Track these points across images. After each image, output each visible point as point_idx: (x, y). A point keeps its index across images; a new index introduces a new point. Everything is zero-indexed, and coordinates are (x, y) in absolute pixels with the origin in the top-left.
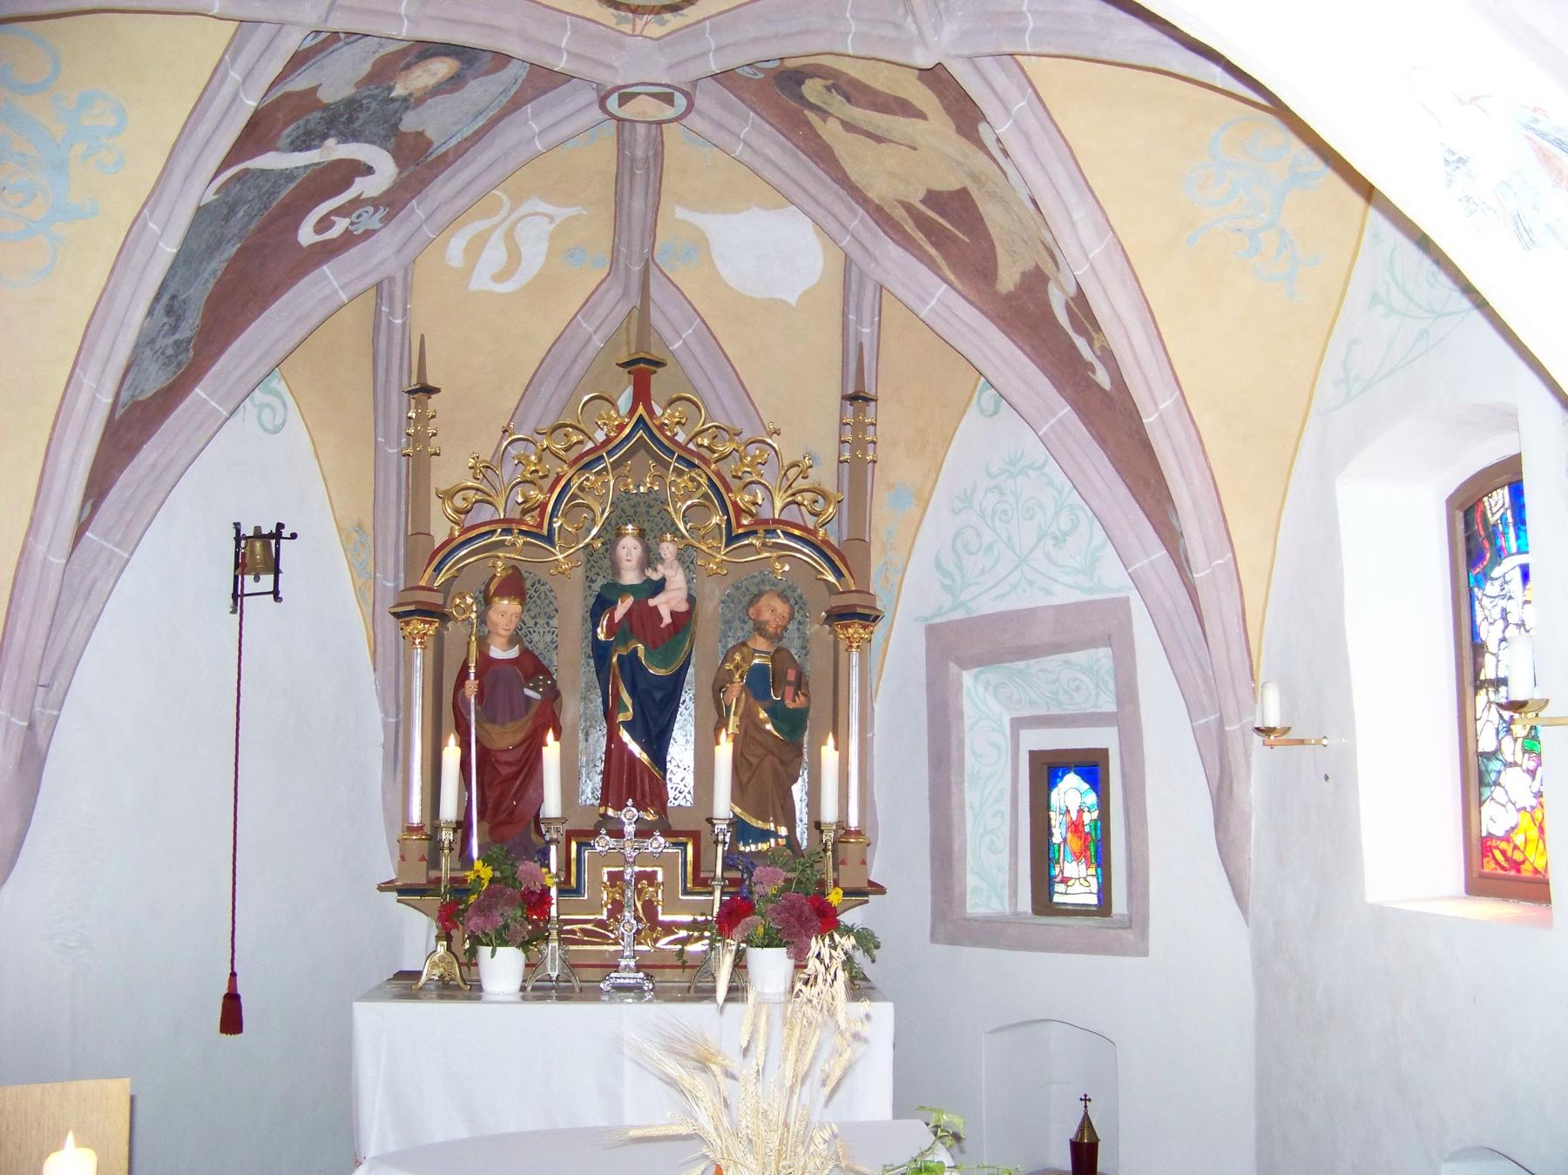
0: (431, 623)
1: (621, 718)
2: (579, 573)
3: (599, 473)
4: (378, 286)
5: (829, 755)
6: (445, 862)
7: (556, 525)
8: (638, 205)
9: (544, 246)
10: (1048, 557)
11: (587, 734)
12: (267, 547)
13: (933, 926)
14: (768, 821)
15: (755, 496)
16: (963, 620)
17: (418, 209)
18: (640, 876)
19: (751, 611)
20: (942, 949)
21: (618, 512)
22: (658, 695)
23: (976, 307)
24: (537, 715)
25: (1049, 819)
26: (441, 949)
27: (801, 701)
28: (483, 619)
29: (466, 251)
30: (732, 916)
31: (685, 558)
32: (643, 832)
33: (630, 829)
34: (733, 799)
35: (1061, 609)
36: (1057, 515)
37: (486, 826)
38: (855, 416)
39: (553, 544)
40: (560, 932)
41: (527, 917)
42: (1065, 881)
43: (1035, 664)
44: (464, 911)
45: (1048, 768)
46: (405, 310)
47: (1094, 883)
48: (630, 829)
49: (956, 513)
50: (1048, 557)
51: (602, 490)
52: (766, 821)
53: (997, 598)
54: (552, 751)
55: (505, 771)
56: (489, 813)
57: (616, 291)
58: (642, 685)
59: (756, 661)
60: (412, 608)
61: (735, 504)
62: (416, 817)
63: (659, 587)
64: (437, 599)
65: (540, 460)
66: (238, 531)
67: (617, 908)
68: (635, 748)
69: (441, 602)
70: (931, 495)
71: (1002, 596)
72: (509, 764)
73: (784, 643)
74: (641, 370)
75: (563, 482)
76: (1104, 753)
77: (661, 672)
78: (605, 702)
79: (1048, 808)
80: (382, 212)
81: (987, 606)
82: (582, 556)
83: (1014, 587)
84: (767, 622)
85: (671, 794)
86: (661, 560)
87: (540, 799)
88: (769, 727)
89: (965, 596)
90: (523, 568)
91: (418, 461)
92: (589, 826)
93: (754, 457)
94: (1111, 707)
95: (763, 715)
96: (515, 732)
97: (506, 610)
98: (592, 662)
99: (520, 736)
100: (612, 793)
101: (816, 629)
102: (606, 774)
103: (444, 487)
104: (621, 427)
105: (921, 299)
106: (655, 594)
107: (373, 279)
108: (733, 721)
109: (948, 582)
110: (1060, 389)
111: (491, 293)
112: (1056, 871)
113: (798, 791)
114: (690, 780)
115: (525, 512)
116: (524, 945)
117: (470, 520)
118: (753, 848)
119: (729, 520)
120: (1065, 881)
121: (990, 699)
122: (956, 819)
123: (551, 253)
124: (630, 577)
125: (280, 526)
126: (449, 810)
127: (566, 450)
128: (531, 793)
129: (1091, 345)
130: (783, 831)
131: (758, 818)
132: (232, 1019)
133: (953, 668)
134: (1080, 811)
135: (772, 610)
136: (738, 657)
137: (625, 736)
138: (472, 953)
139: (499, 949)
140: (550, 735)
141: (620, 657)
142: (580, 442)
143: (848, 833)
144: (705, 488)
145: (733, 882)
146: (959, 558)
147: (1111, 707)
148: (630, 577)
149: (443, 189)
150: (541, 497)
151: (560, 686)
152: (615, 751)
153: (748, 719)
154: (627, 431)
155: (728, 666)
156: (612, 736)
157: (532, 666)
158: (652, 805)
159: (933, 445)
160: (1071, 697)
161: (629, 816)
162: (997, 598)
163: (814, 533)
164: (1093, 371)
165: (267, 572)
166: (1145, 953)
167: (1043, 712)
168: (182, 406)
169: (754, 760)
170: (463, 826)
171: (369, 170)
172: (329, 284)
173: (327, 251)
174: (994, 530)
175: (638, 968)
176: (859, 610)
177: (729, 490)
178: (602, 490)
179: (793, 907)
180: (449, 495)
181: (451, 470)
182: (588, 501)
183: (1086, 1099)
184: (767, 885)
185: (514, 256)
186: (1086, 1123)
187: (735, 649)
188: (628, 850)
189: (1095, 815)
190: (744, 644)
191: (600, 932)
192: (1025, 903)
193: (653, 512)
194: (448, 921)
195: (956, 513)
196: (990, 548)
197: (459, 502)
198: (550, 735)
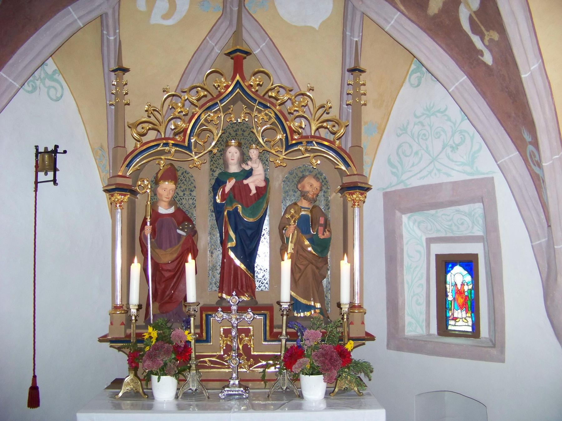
0: (125, 195)
1: (229, 245)
2: (207, 167)
3: (215, 112)
5: (345, 265)
7: (192, 141)
10: (449, 157)
11: (212, 253)
14: (310, 300)
15: (301, 123)
16: (403, 190)
19: (299, 186)
20: (393, 353)
21: (227, 134)
22: (249, 232)
23: (416, 24)
24: (184, 244)
25: (446, 288)
30: (292, 357)
31: (263, 157)
33: (234, 308)
34: (292, 289)
36: (453, 135)
37: (157, 305)
38: (355, 79)
39: (191, 152)
41: (180, 360)
43: (440, 212)
44: (143, 355)
45: (445, 263)
48: (234, 308)
49: (398, 136)
50: (449, 157)
51: (218, 120)
53: (421, 178)
54: (190, 265)
55: (167, 274)
56: (159, 298)
57: (225, 24)
58: (241, 227)
59: (303, 213)
60: (114, 187)
61: (290, 128)
62: (119, 302)
63: (249, 173)
64: (129, 182)
65: (183, 106)
66: (37, 150)
68: (238, 262)
69: (130, 183)
70: (384, 129)
71: (423, 178)
72: (170, 271)
73: (317, 203)
74: (238, 56)
75: (196, 117)
76: (476, 256)
77: (251, 220)
78: (221, 236)
81: (416, 182)
82: (207, 158)
83: (430, 173)
84: (308, 192)
85: (257, 284)
86: (250, 159)
88: (310, 249)
89: (404, 177)
90: (176, 165)
91: (118, 105)
93: (300, 102)
94: (481, 233)
95: (307, 243)
96: (171, 254)
97: (167, 188)
98: (214, 214)
99: (175, 256)
101: (335, 197)
104: (227, 87)
105: (385, 20)
106: (247, 177)
108: (291, 246)
109: (394, 170)
110: (461, 67)
114: (267, 276)
115: (176, 134)
116: (175, 375)
117: (145, 139)
118: (302, 315)
119: (287, 136)
120: (455, 319)
122: (399, 289)
124: (234, 168)
125: (56, 147)
127: (198, 100)
129: (482, 39)
130: (318, 305)
131: (304, 298)
132: (34, 399)
133: (398, 213)
134: (463, 285)
136: (292, 211)
137: (232, 255)
139: (163, 378)
140: (190, 257)
141: (228, 212)
142: (205, 96)
144: (273, 120)
146: (400, 158)
148: (234, 168)
150: (184, 125)
151: (197, 228)
152: (226, 262)
153: (299, 245)
154: (230, 89)
155: (288, 216)
156: (225, 254)
157: (182, 217)
158: (247, 292)
159: (387, 103)
160: (458, 228)
161: (233, 300)
162: (421, 178)
163: (333, 142)
164: (482, 55)
165: (50, 170)
166: (503, 361)
167: (442, 235)
169: (302, 267)
174: (419, 144)
176: (359, 185)
177: (286, 120)
178: (218, 120)
179: (327, 354)
181: (135, 112)
182: (210, 127)
184: (311, 339)
187: (290, 207)
189: (470, 287)
190: (295, 204)
191: (220, 362)
192: (434, 329)
193: (246, 134)
195: (398, 136)
196: (417, 153)
197: (139, 129)
198: (190, 257)
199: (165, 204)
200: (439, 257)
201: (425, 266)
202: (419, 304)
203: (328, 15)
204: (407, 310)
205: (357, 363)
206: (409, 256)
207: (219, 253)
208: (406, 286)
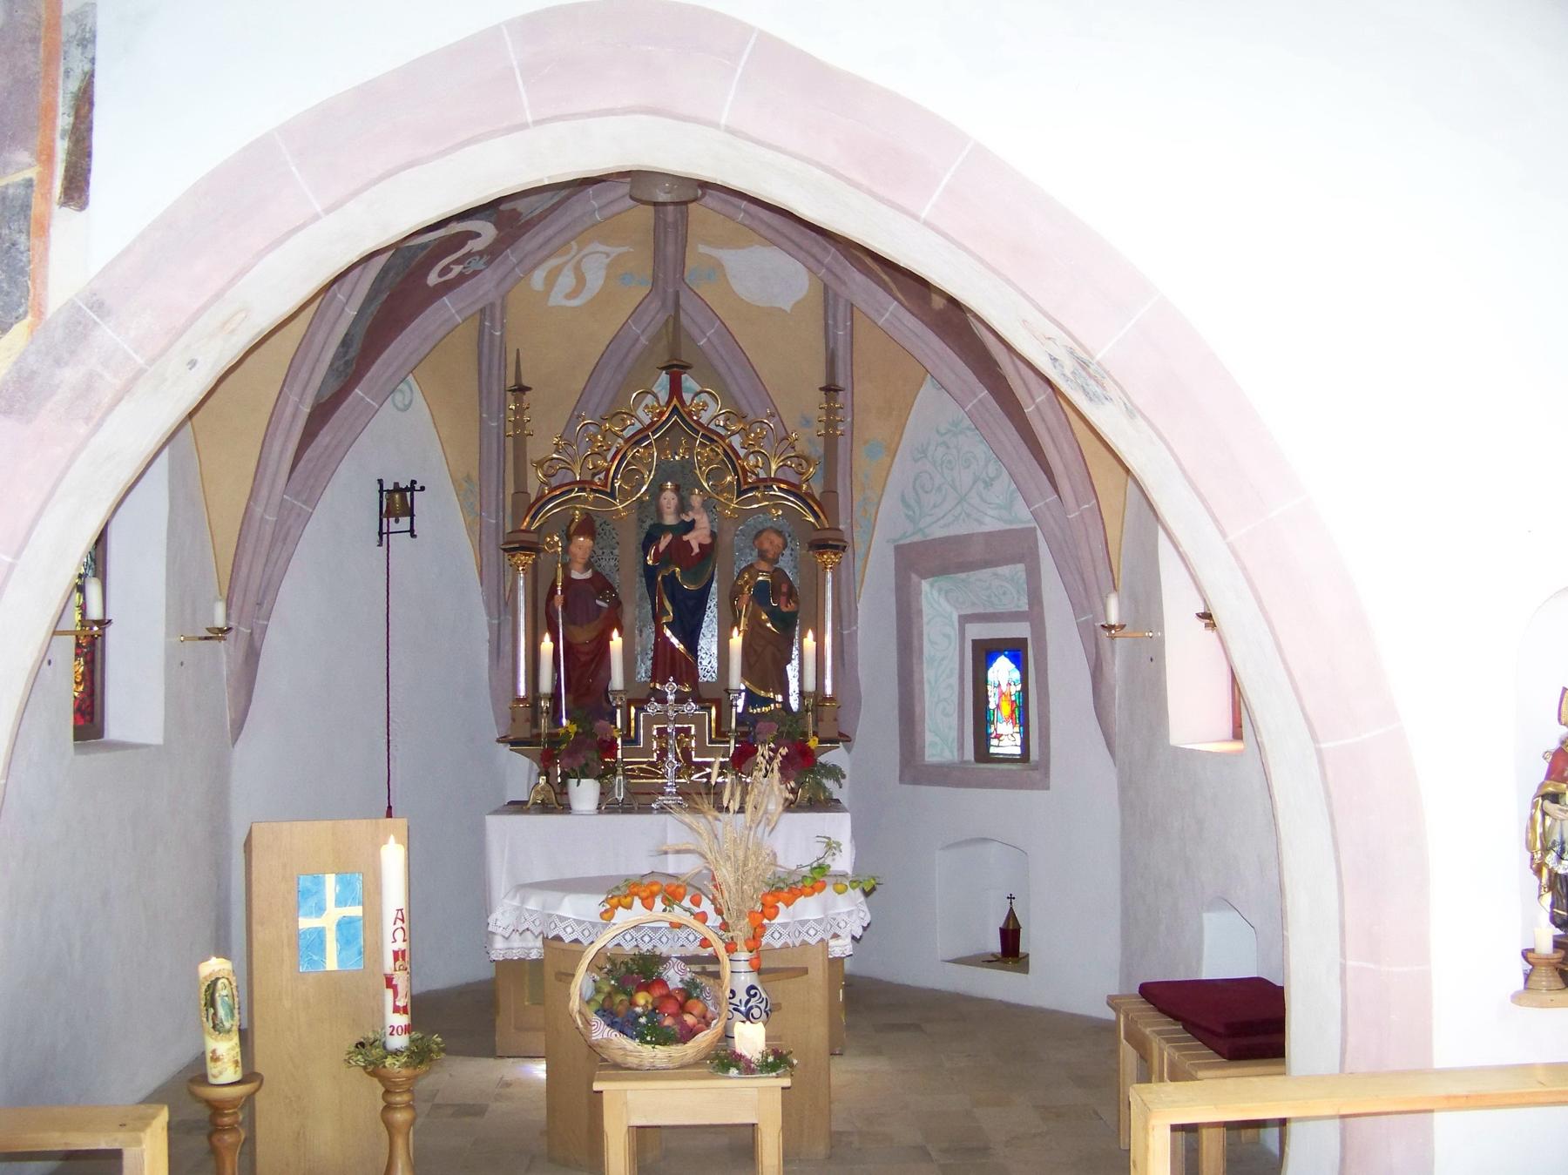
4: (483, 311)
5: (809, 642)
6: (544, 722)
8: (670, 249)
9: (603, 273)
12: (403, 498)
13: (902, 772)
17: (511, 256)
18: (678, 731)
20: (909, 788)
22: (690, 603)
26: (543, 780)
27: (791, 607)
28: (566, 550)
29: (546, 278)
31: (708, 506)
32: (681, 699)
33: (671, 697)
35: (990, 534)
40: (624, 771)
42: (998, 737)
46: (503, 325)
47: (1018, 738)
48: (671, 697)
52: (767, 691)
54: (616, 642)
55: (583, 659)
57: (655, 305)
61: (743, 468)
62: (522, 693)
63: (690, 526)
64: (533, 538)
67: (663, 753)
68: (674, 641)
73: (781, 564)
77: (692, 588)
79: (986, 682)
80: (485, 258)
81: (938, 532)
85: (701, 673)
86: (692, 508)
87: (609, 678)
92: (644, 696)
94: (1026, 608)
95: (764, 617)
99: (594, 634)
100: (658, 674)
102: (655, 659)
103: (539, 456)
104: (661, 414)
107: (479, 306)
111: (562, 307)
112: (992, 730)
113: (792, 670)
120: (998, 737)
121: (942, 601)
122: (917, 691)
123: (607, 277)
124: (670, 520)
125: (413, 482)
126: (546, 685)
128: (602, 674)
130: (779, 698)
133: (914, 577)
135: (771, 542)
137: (668, 633)
138: (564, 784)
140: (615, 633)
143: (825, 699)
145: (744, 734)
147: (1026, 608)
148: (670, 520)
149: (529, 242)
152: (661, 644)
155: (740, 582)
156: (659, 633)
157: (601, 584)
159: (898, 409)
161: (670, 689)
167: (981, 610)
168: (345, 405)
170: (555, 697)
171: (478, 235)
172: (450, 308)
173: (446, 288)
175: (678, 794)
180: (540, 464)
181: (542, 445)
183: (1011, 898)
185: (581, 280)
186: (1011, 915)
188: (670, 713)
189: (1019, 687)
192: (969, 754)
194: (546, 763)
198: (615, 633)
199: (578, 566)
200: (976, 644)
201: (957, 659)
202: (947, 715)
203: (804, 292)
204: (928, 723)
205: (823, 766)
206: (932, 643)
207: (650, 633)
208: (926, 687)
